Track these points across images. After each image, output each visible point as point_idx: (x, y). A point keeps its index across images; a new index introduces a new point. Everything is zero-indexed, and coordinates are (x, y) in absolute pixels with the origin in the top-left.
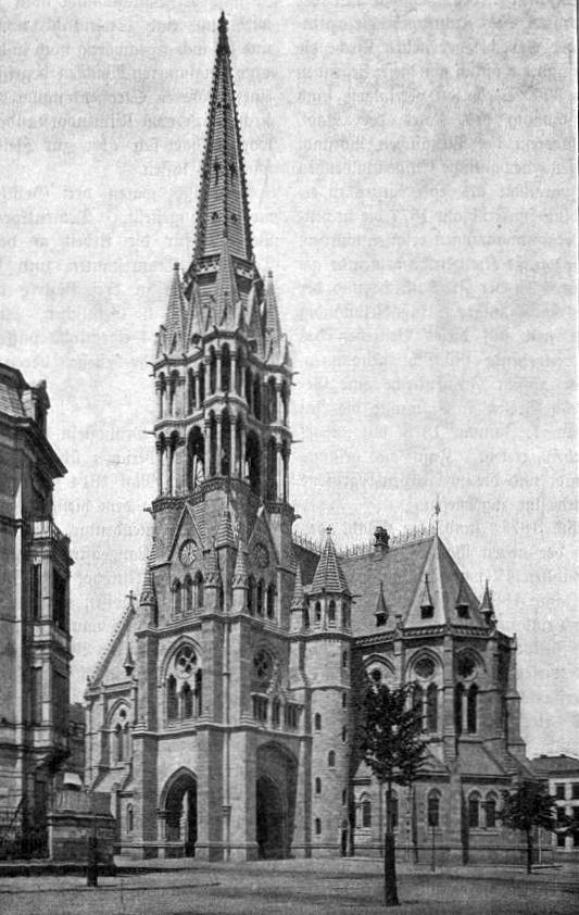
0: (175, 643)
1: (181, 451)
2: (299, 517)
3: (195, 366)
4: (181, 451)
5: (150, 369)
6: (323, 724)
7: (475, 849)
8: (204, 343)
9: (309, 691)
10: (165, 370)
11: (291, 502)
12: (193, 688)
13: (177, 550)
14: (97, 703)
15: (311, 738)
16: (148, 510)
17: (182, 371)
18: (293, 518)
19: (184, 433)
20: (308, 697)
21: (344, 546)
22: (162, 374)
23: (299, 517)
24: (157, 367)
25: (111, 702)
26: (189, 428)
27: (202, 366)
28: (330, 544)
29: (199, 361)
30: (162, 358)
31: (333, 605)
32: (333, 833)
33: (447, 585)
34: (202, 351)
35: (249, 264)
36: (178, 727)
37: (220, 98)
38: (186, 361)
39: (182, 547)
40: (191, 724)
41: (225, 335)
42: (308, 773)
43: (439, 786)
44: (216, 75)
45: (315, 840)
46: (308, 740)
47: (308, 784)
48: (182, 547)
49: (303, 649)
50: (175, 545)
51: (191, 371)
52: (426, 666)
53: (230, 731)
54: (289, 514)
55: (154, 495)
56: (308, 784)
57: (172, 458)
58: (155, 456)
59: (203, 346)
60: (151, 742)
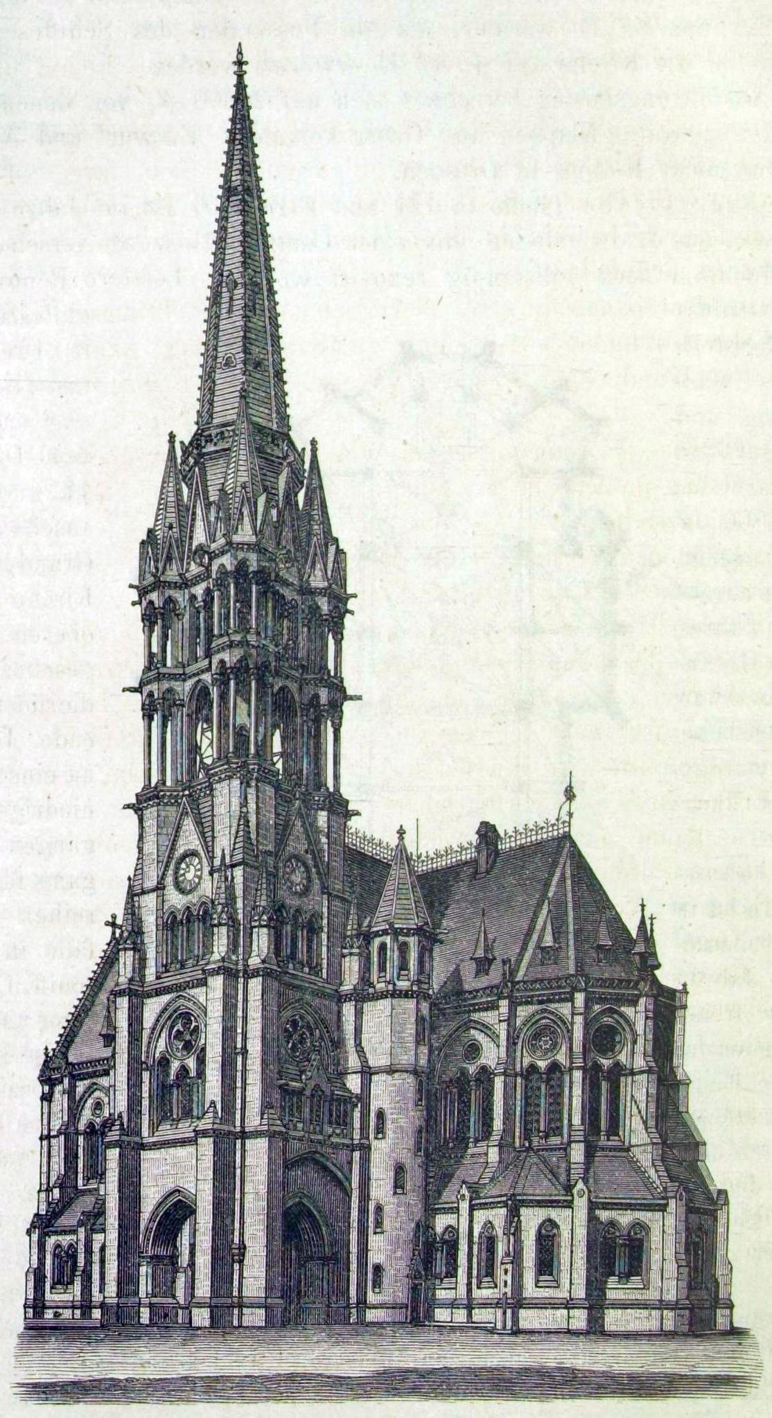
0: (168, 1004)
2: (358, 814)
3: (199, 590)
5: (134, 595)
8: (211, 559)
9: (367, 1073)
10: (154, 596)
11: (346, 792)
12: (193, 1074)
13: (172, 867)
15: (369, 1147)
16: (128, 806)
17: (181, 597)
18: (348, 814)
20: (366, 1085)
21: (362, 832)
22: (151, 602)
23: (358, 814)
24: (143, 591)
25: (81, 1086)
26: (189, 684)
27: (208, 592)
28: (401, 848)
29: (203, 585)
31: (403, 948)
32: (394, 1289)
33: (319, 643)
34: (208, 568)
35: (283, 435)
36: (167, 1131)
37: (236, 179)
39: (309, 879)
40: (185, 1129)
41: (240, 546)
42: (365, 1197)
44: (231, 142)
45: (372, 1298)
46: (366, 1149)
47: (363, 1211)
51: (193, 598)
53: (244, 1135)
54: (339, 808)
55: (137, 785)
56: (363, 1211)
59: (210, 564)
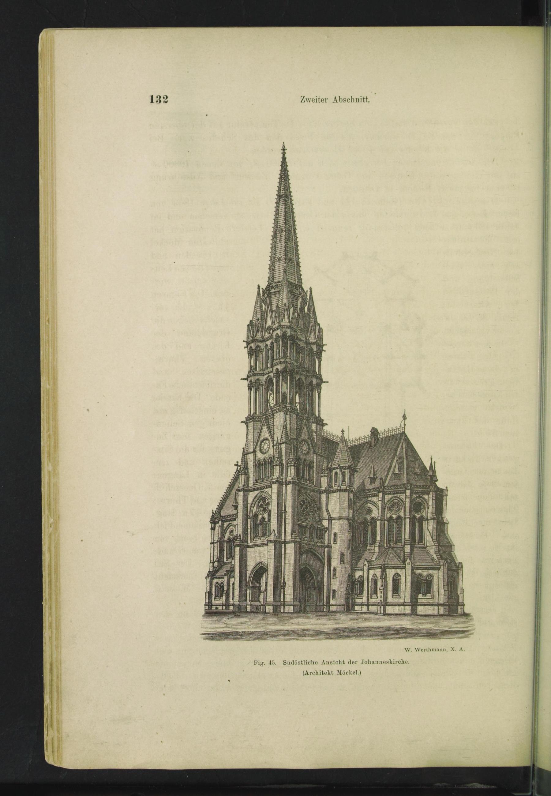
0: (257, 494)
1: (262, 389)
2: (327, 425)
3: (269, 343)
4: (262, 389)
6: (337, 596)
7: (408, 545)
9: (330, 519)
10: (252, 345)
11: (322, 416)
13: (259, 444)
14: (217, 525)
16: (243, 422)
17: (262, 345)
18: (323, 425)
19: (263, 379)
20: (330, 524)
23: (327, 425)
24: (248, 343)
26: (265, 377)
27: (272, 343)
28: (343, 437)
29: (270, 341)
30: (251, 339)
31: (344, 474)
32: (340, 599)
34: (272, 335)
36: (257, 541)
37: (282, 192)
38: (264, 340)
40: (264, 540)
42: (329, 565)
43: (399, 571)
46: (330, 547)
47: (329, 570)
48: (261, 443)
49: (327, 498)
50: (258, 441)
51: (267, 345)
52: (396, 505)
54: (320, 422)
57: (256, 392)
58: (247, 391)
60: (244, 548)
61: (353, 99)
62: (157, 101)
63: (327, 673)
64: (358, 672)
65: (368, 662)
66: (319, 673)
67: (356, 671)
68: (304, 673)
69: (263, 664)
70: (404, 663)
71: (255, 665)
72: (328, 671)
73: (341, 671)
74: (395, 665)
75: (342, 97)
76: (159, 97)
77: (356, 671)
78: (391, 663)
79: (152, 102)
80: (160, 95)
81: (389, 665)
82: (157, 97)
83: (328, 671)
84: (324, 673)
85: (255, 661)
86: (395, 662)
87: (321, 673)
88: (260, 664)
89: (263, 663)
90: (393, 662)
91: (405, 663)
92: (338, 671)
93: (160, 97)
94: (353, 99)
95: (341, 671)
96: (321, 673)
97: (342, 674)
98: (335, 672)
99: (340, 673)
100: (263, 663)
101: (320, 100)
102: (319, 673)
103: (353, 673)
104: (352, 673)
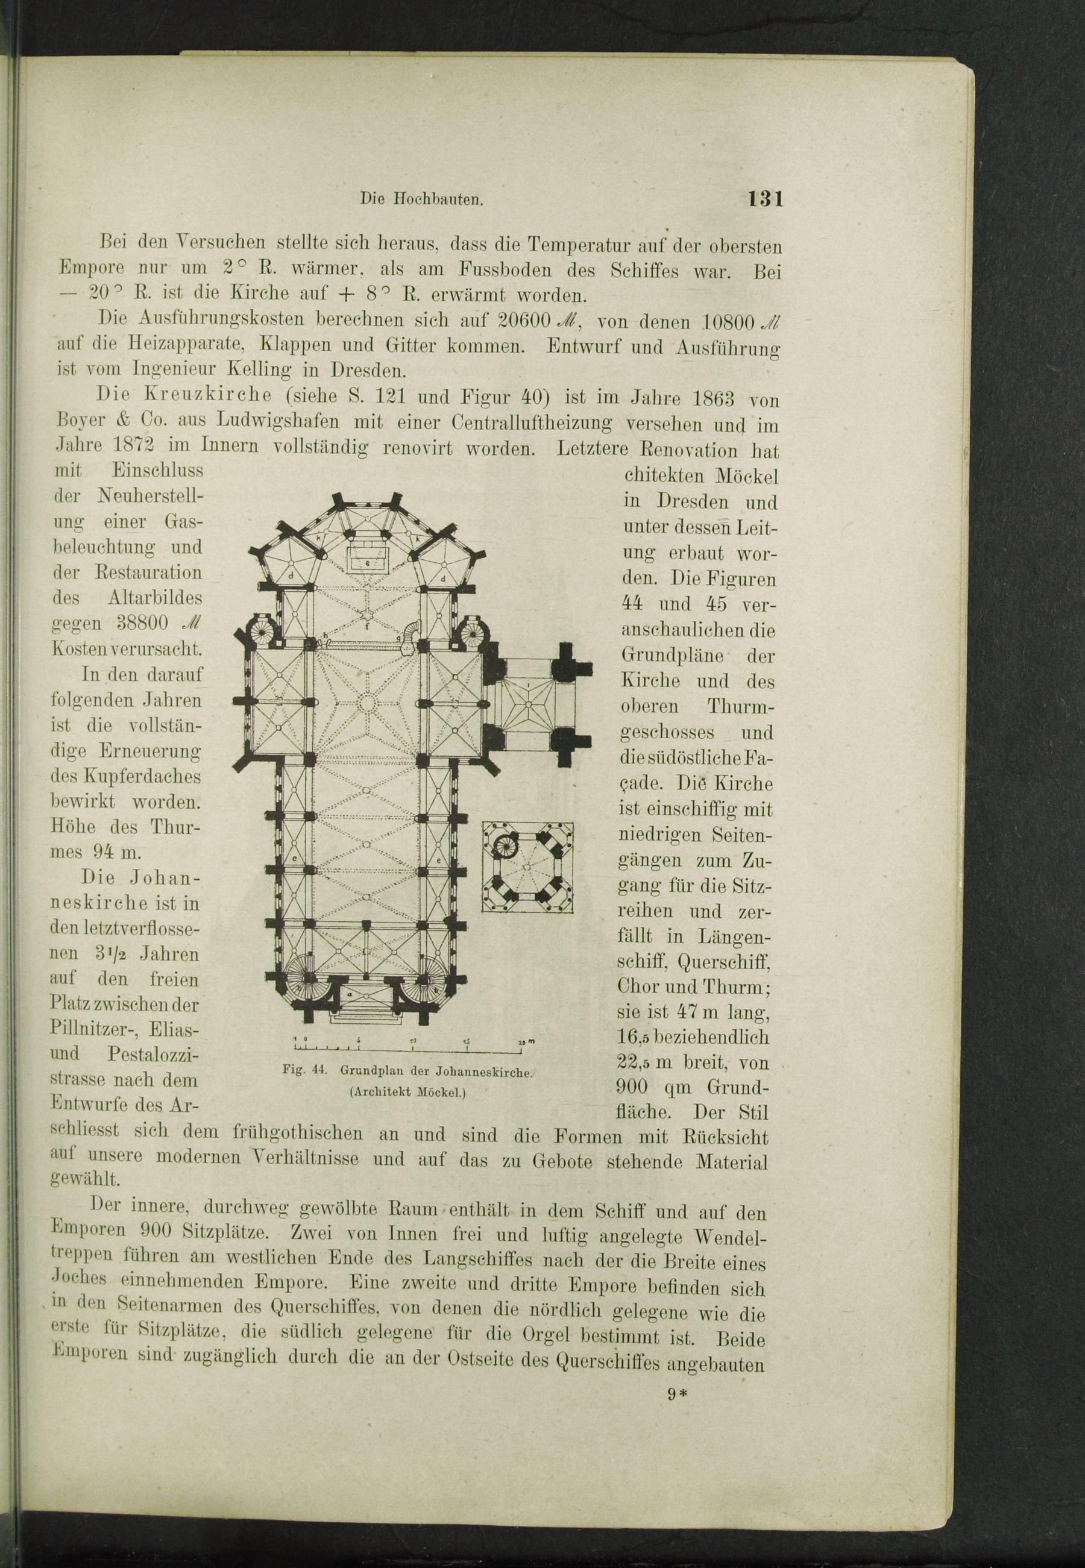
61: (427, 199)
62: (762, 202)
63: (399, 1091)
64: (460, 1092)
65: (450, 1073)
66: (382, 1093)
67: (457, 1089)
68: (353, 1094)
69: (302, 1071)
70: (478, 1075)
71: (285, 1072)
72: (443, 1088)
73: (425, 1088)
74: (504, 1078)
75: (439, 194)
76: (765, 193)
77: (457, 1089)
78: (495, 1074)
79: (752, 204)
80: (768, 190)
81: (492, 1079)
82: (763, 194)
83: (443, 1088)
84: (391, 1092)
85: (285, 1065)
86: (504, 1074)
87: (387, 1093)
88: (295, 1071)
89: (301, 1068)
90: (499, 1074)
91: (523, 1075)
92: (420, 1088)
93: (769, 194)
94: (427, 199)
95: (425, 1088)
96: (387, 1093)
97: (427, 1093)
98: (414, 1091)
99: (423, 1092)
100: (301, 1068)
101: (462, 200)
102: (382, 1093)
103: (450, 1094)
104: (447, 1093)
